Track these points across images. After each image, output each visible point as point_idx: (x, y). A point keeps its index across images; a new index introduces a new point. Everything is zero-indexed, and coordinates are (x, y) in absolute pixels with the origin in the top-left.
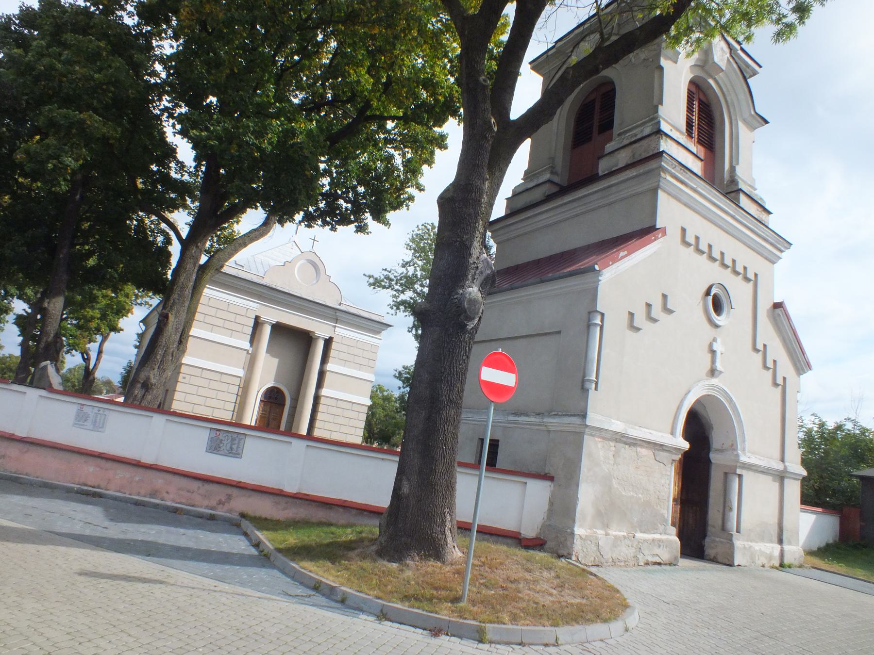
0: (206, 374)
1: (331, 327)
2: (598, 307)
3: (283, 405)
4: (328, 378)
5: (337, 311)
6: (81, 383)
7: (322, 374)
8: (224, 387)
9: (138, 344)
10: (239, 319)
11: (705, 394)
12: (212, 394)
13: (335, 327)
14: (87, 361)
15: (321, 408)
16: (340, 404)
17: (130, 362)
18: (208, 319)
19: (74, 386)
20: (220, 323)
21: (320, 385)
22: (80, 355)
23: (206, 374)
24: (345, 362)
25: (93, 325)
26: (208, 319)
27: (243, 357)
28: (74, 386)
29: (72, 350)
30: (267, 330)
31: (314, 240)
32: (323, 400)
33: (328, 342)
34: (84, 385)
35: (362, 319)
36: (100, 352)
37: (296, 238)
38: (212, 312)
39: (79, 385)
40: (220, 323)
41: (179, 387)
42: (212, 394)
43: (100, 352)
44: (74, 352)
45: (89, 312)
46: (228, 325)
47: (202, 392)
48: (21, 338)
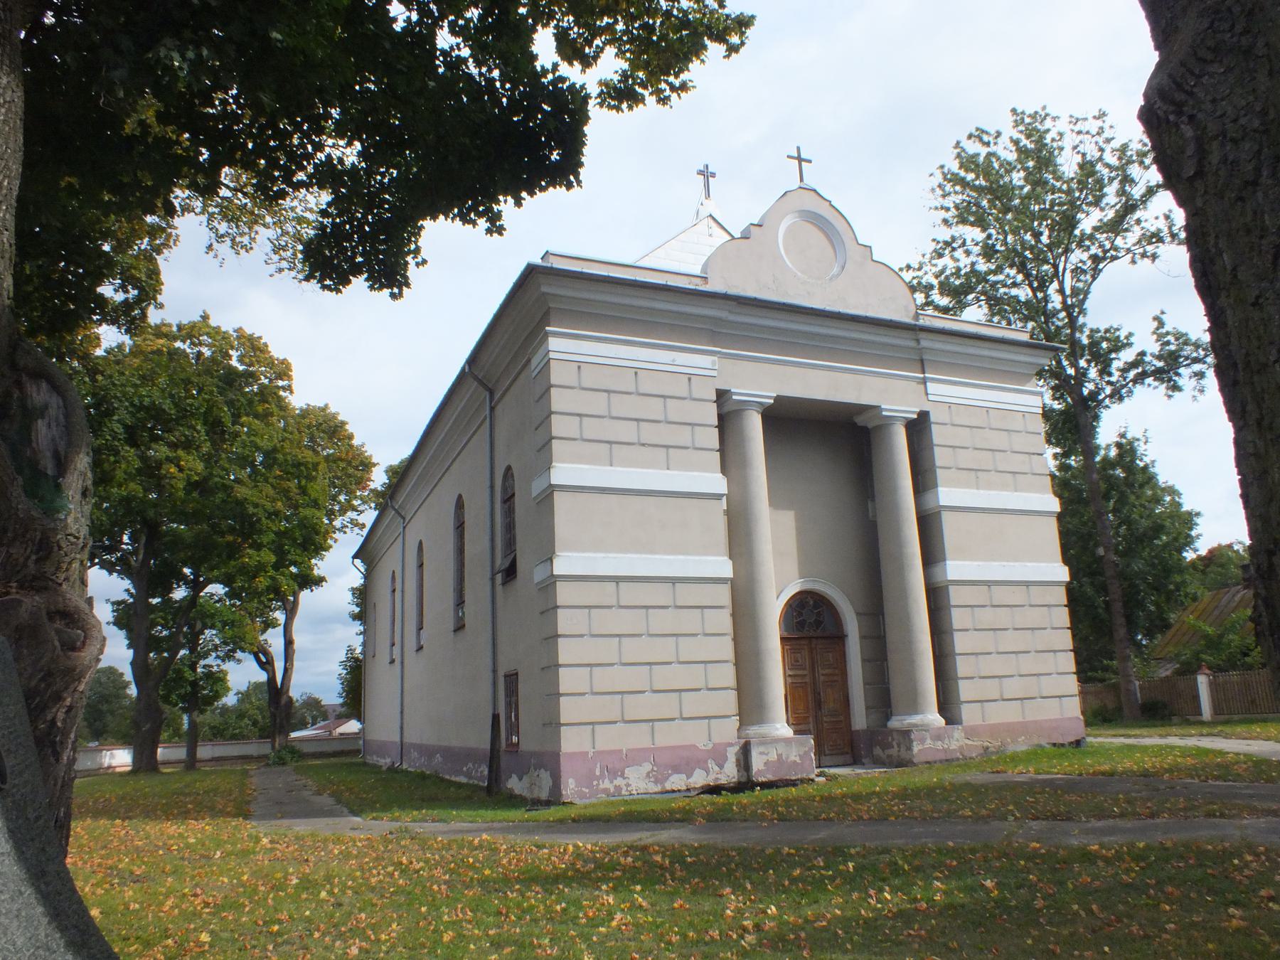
0: (630, 594)
1: (914, 384)
2: (934, 437)
3: (839, 638)
4: (951, 528)
5: (922, 335)
6: (268, 714)
7: (929, 524)
8: (690, 621)
9: (357, 610)
10: (676, 410)
11: (797, 590)
12: (662, 650)
13: (924, 382)
14: (267, 666)
15: (958, 618)
16: (1000, 595)
17: (351, 650)
18: (592, 429)
19: (255, 723)
20: (626, 431)
21: (932, 554)
22: (252, 657)
23: (630, 594)
24: (975, 475)
25: (262, 582)
26: (592, 429)
27: (717, 515)
28: (255, 723)
29: (234, 651)
30: (754, 425)
31: (800, 159)
32: (956, 596)
33: (918, 427)
34: (273, 716)
35: (987, 344)
36: (289, 643)
37: (711, 207)
38: (597, 403)
39: (264, 718)
40: (626, 431)
41: (567, 651)
42: (662, 650)
43: (289, 643)
44: (239, 655)
45: (250, 557)
46: (650, 433)
47: (633, 651)
48: (131, 651)
